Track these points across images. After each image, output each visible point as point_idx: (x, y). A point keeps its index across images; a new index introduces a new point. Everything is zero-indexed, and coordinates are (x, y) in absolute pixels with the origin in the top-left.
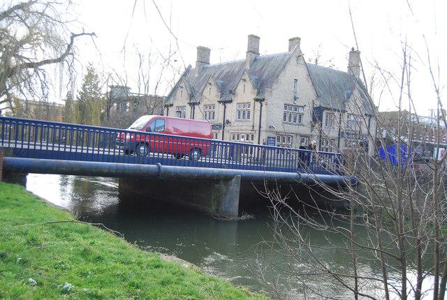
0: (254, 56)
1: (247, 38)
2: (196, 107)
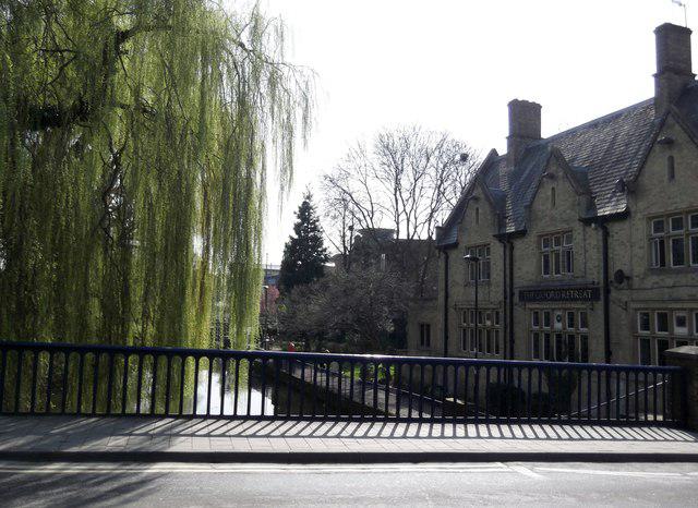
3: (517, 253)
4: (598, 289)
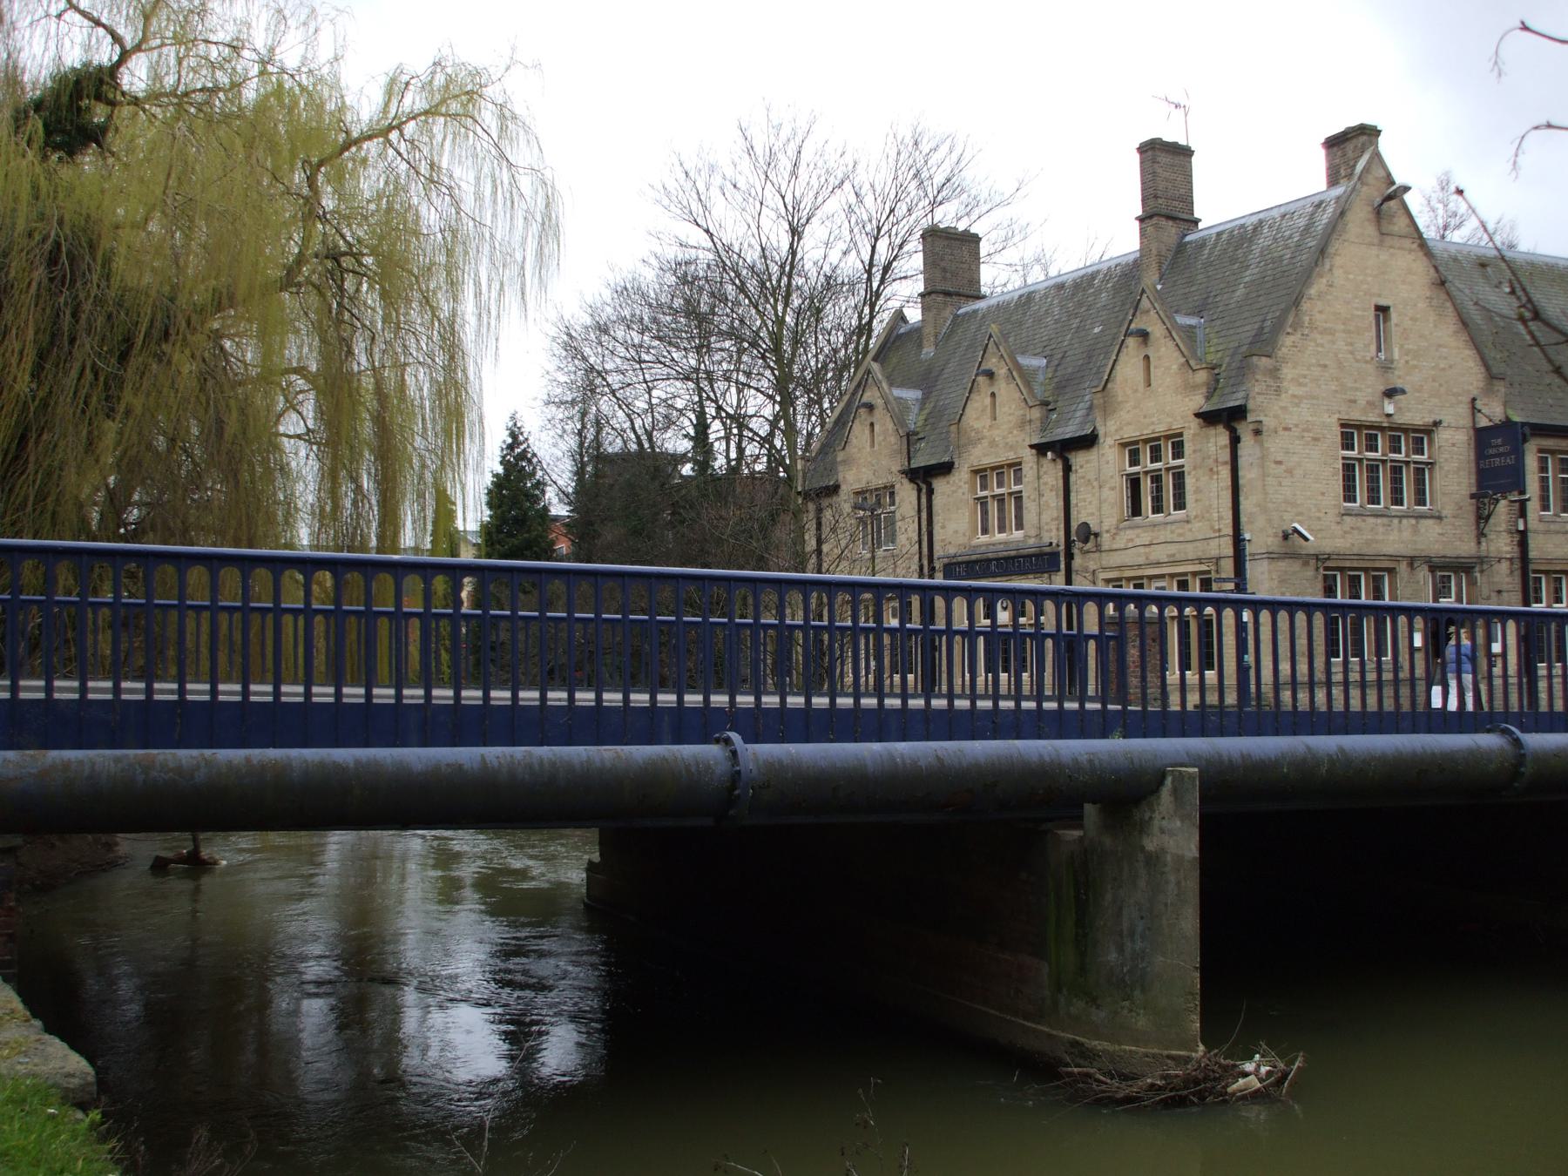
0: (1171, 231)
1: (1136, 158)
2: (940, 485)
3: (938, 500)
4: (1057, 554)
